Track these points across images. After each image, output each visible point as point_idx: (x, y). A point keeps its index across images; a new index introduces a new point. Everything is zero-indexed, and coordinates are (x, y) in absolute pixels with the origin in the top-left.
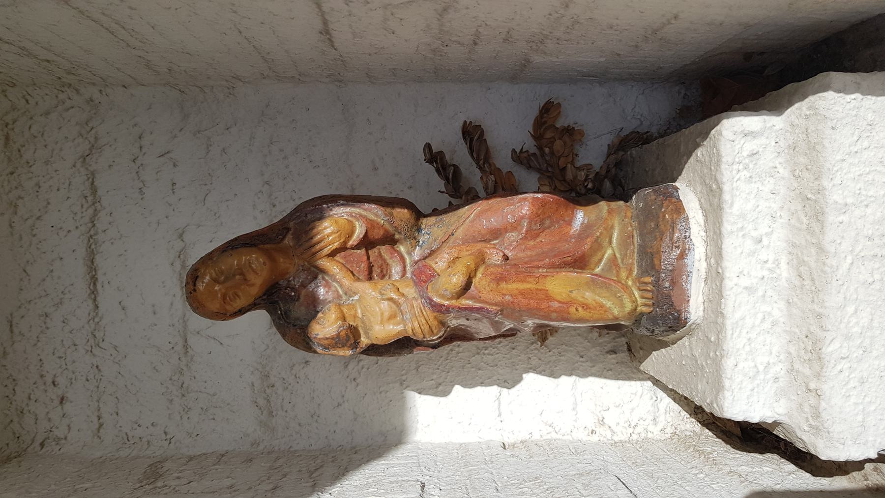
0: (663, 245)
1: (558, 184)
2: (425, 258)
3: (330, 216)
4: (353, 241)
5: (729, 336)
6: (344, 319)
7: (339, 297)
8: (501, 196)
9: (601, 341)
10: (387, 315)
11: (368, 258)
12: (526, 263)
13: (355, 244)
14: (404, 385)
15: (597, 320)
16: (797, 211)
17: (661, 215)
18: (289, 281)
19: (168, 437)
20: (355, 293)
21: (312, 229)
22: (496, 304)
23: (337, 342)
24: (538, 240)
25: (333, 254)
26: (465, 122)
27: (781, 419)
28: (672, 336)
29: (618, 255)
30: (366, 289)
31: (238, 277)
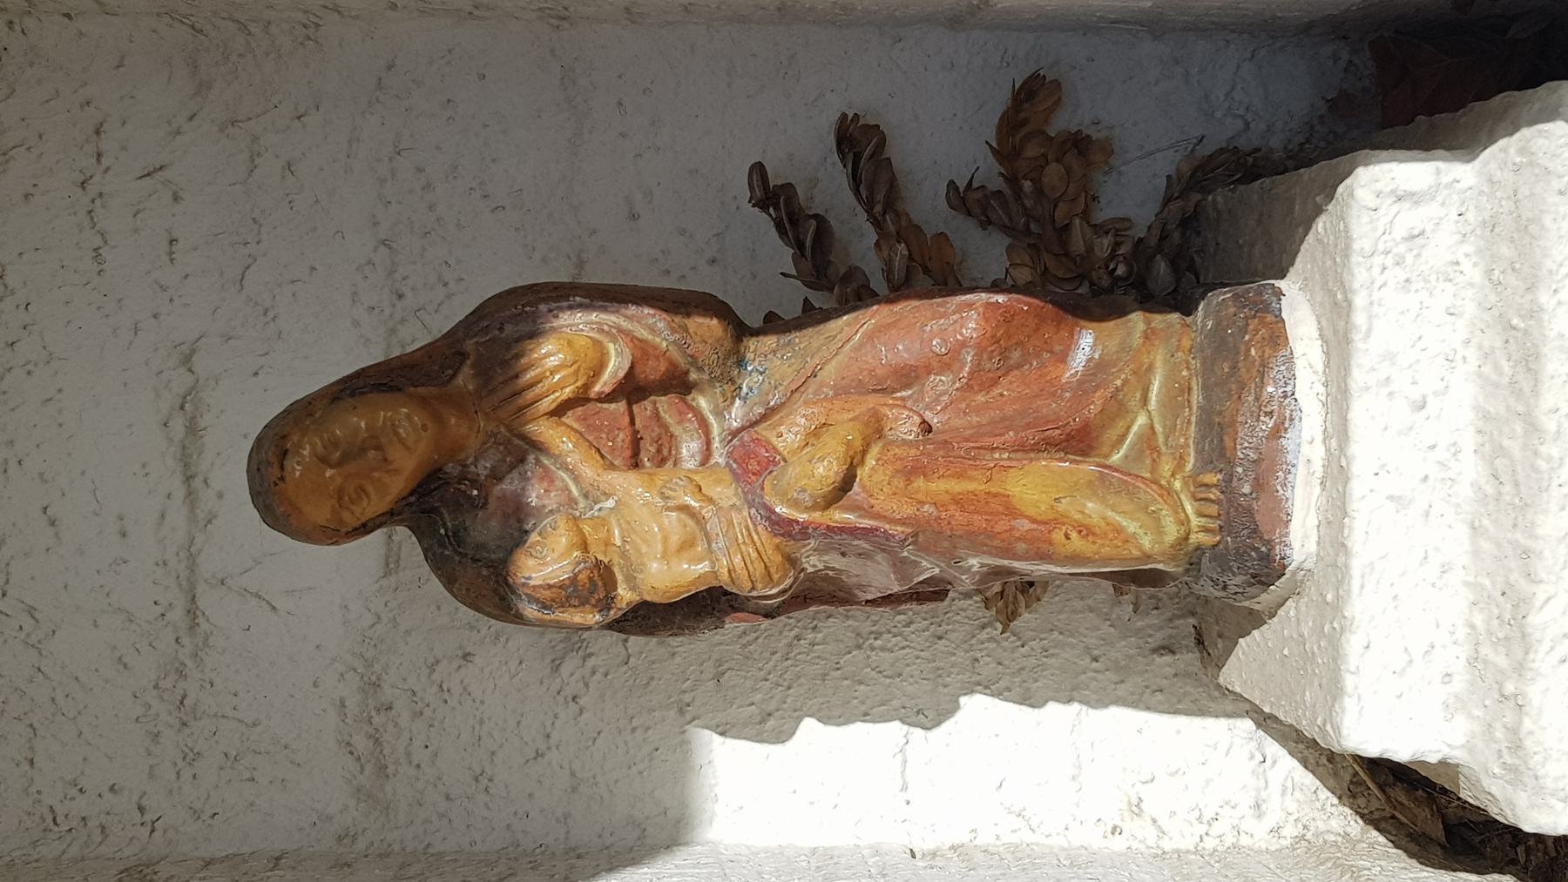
0: (1244, 409)
1: (1051, 263)
2: (754, 424)
3: (553, 329)
4: (604, 384)
5: (1355, 589)
6: (584, 546)
7: (572, 502)
8: (920, 297)
9: (1140, 624)
10: (675, 540)
11: (632, 422)
12: (967, 440)
13: (607, 390)
14: (686, 713)
15: (1106, 561)
16: (1493, 348)
17: (1243, 348)
18: (465, 466)
19: (148, 818)
20: (607, 495)
21: (518, 356)
22: (902, 522)
23: (570, 593)
24: (996, 391)
25: (559, 411)
26: (844, 116)
27: (1457, 755)
28: (1265, 599)
29: (1158, 428)
30: (630, 487)
31: (371, 454)
